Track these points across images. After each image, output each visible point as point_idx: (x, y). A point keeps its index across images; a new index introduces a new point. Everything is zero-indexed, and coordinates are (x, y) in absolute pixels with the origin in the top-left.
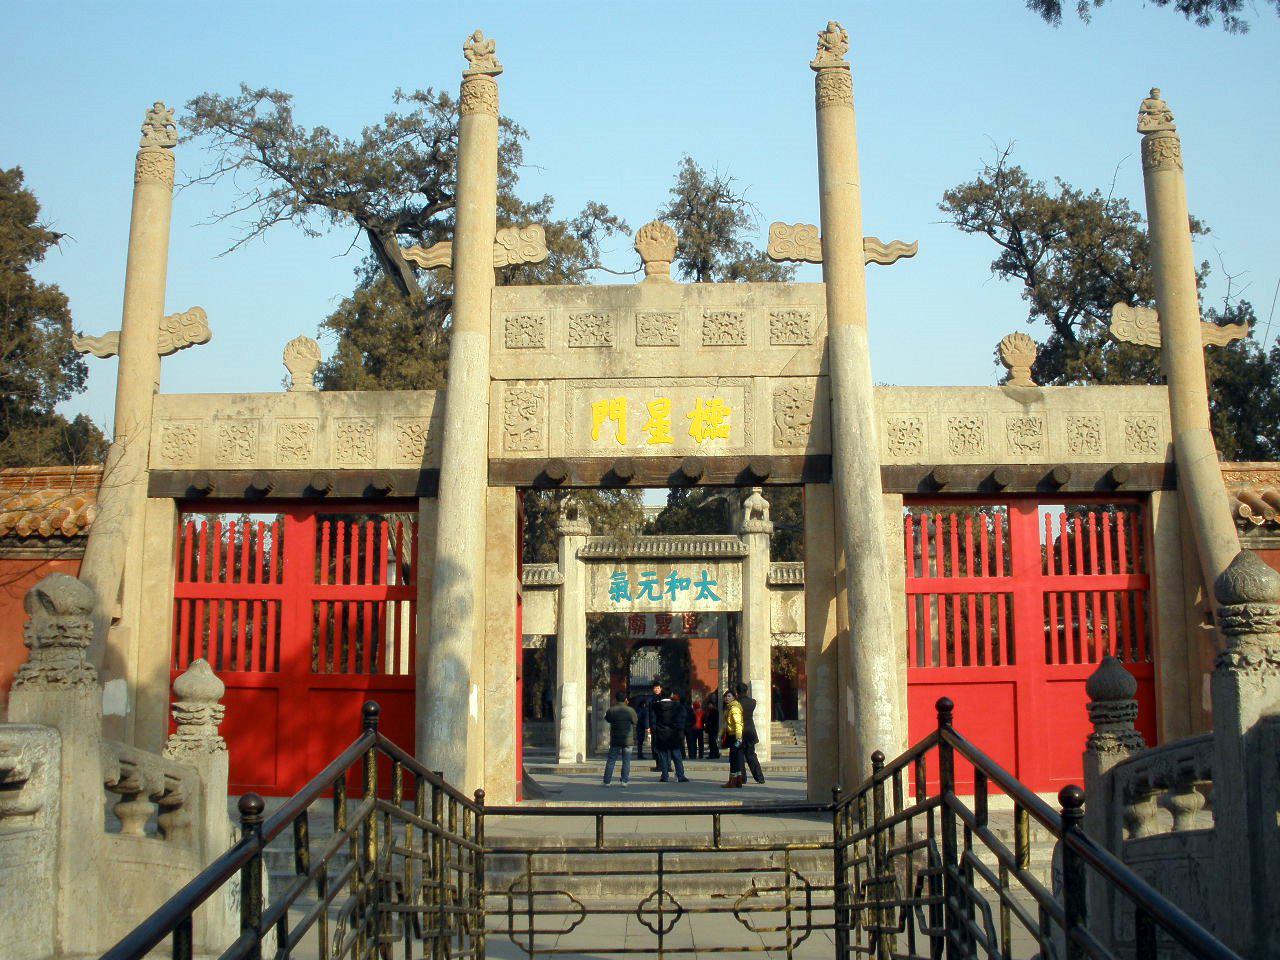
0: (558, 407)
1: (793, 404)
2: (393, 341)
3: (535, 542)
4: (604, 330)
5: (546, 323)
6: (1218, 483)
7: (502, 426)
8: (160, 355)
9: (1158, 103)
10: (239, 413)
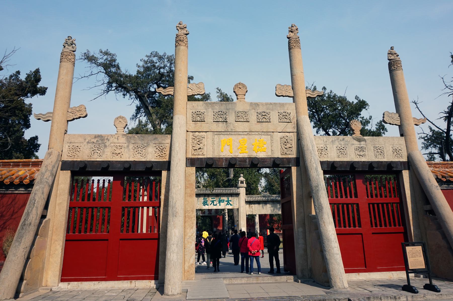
0: (210, 141)
1: (286, 141)
4: (225, 116)
5: (205, 113)
7: (191, 147)
8: (68, 121)
10: (97, 141)
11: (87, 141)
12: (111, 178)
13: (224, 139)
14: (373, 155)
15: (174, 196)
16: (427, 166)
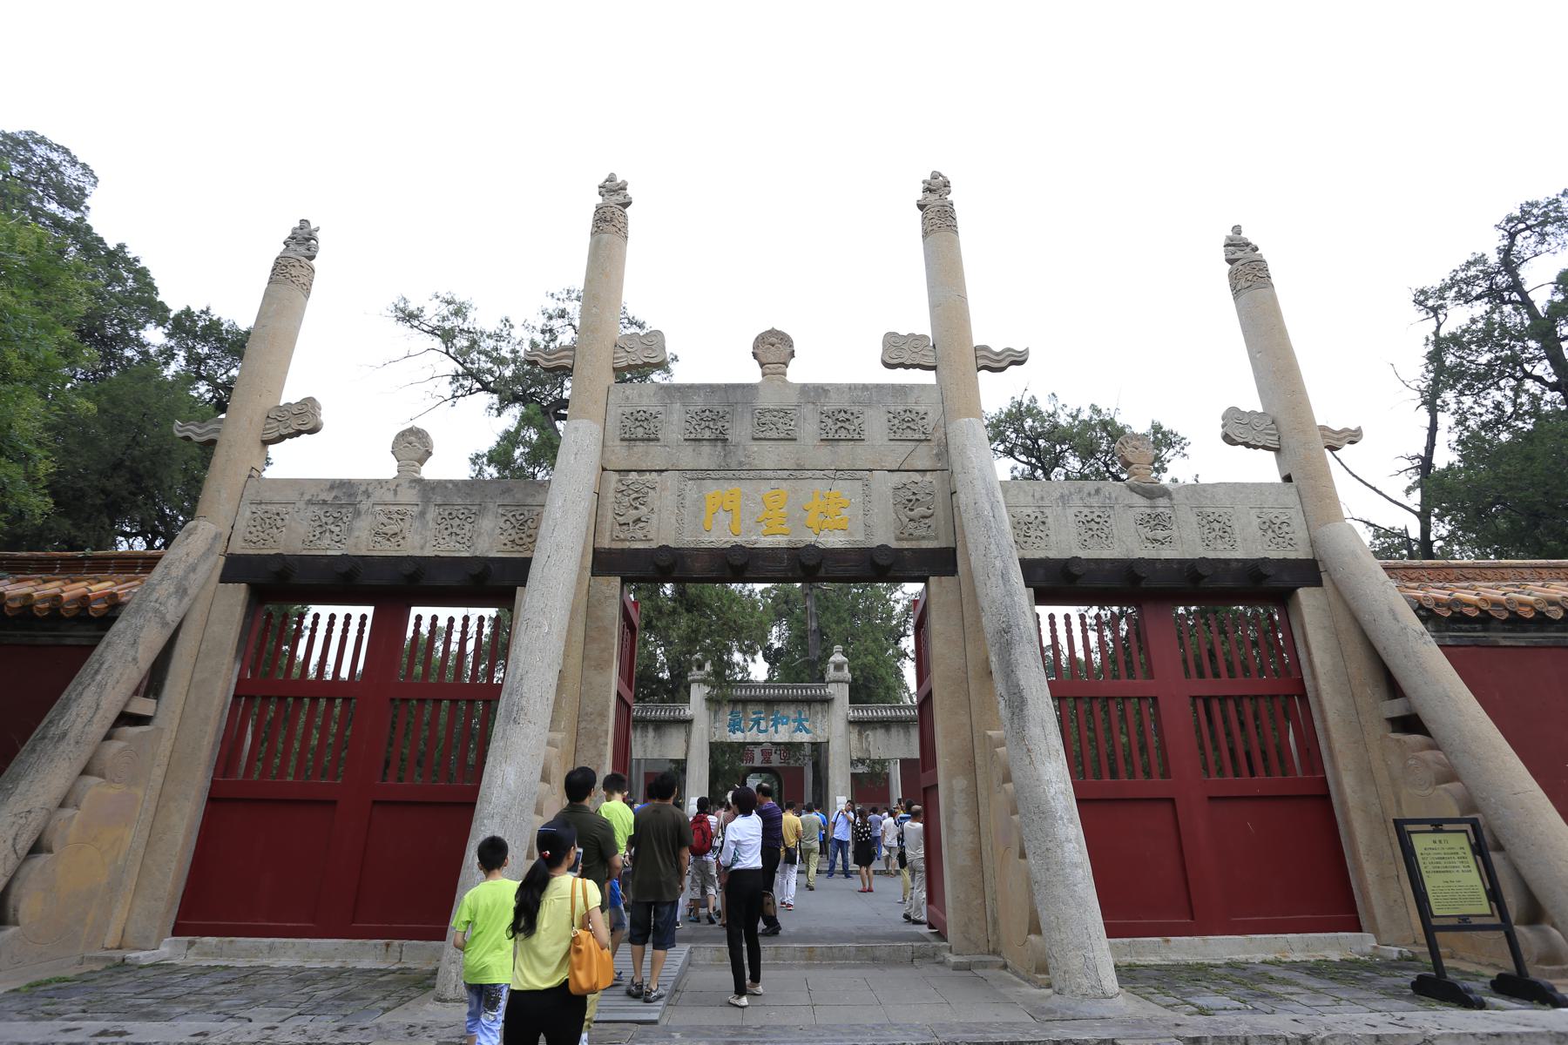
0: (669, 499)
7: (610, 515)
11: (307, 497)
12: (369, 611)
13: (715, 491)
14: (1198, 540)
15: (522, 657)
16: (1383, 575)
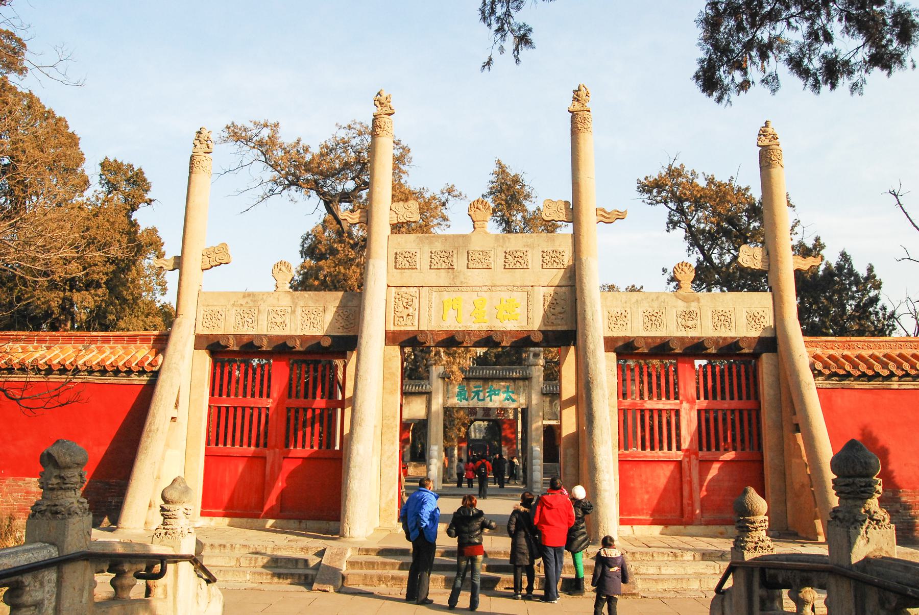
2: (332, 264)
3: (414, 376)
5: (418, 255)
6: (802, 350)
9: (769, 130)
